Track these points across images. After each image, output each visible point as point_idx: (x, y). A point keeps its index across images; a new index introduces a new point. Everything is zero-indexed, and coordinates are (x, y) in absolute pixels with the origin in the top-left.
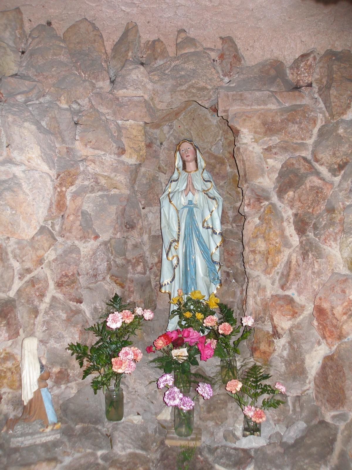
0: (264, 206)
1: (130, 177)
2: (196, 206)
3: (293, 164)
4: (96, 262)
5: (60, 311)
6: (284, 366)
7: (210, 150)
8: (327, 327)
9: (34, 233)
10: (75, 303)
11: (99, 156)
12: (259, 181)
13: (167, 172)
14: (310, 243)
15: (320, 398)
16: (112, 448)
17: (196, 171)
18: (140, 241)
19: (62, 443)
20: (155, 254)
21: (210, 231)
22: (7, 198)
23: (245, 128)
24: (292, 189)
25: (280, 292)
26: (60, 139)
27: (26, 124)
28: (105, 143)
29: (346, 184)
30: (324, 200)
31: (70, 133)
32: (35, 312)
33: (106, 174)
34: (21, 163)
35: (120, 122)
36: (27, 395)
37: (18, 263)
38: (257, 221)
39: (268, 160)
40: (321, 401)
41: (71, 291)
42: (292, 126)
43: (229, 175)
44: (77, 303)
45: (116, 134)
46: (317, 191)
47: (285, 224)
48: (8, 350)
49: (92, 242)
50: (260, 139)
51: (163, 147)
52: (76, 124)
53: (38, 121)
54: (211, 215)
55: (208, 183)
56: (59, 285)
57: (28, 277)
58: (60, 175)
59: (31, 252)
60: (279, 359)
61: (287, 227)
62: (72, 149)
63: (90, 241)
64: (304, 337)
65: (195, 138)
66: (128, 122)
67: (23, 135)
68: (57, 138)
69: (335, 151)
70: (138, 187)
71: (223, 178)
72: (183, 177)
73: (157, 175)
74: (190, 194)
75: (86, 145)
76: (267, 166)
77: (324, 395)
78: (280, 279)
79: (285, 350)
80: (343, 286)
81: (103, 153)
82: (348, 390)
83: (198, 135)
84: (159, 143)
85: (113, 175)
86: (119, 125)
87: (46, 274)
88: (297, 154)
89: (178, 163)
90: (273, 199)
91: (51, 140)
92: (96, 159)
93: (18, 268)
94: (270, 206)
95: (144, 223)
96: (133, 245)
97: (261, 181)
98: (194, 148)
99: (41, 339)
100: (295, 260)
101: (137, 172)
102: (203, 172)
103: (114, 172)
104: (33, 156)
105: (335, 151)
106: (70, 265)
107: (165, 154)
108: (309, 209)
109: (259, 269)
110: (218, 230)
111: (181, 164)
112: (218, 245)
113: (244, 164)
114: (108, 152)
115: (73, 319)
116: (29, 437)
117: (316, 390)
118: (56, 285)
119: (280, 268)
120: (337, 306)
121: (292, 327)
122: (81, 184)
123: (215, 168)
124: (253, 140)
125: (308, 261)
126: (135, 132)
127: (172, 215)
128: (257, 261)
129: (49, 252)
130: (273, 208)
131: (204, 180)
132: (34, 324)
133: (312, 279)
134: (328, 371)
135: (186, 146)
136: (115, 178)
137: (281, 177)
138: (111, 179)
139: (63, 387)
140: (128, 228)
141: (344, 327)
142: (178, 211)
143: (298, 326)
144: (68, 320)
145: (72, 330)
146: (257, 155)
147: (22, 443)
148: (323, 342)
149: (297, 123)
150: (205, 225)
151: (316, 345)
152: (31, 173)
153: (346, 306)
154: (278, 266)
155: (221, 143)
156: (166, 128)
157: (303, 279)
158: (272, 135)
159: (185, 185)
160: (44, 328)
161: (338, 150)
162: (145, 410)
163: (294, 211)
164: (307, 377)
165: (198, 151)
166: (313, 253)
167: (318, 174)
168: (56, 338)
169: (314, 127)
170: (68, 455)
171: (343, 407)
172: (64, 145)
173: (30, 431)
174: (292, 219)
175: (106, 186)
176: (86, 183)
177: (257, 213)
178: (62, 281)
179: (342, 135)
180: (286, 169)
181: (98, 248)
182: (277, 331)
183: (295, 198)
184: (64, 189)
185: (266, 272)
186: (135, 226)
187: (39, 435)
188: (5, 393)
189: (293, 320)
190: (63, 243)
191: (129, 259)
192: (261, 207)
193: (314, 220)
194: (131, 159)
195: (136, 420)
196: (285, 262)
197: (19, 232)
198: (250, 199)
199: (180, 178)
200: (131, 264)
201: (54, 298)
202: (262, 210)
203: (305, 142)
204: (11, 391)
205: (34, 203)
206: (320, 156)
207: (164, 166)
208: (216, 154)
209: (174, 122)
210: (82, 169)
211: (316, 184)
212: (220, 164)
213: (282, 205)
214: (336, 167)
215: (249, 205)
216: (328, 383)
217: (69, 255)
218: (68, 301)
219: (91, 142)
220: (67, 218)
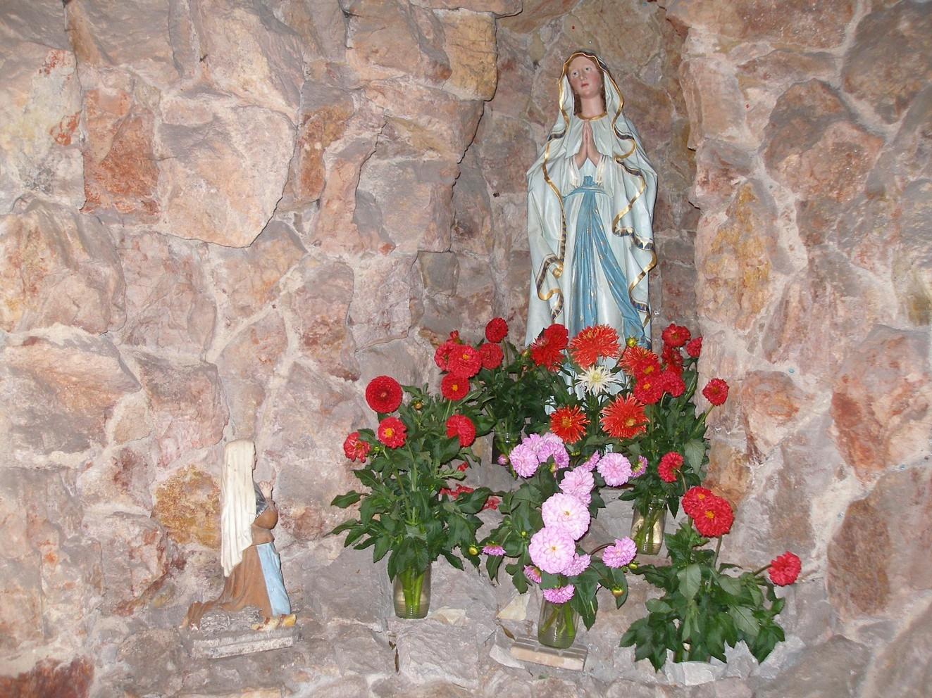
0: (737, 187)
1: (461, 127)
2: (600, 188)
3: (800, 98)
4: (386, 298)
5: (309, 394)
6: (768, 522)
7: (637, 75)
8: (857, 439)
9: (256, 233)
10: (342, 380)
11: (394, 81)
12: (728, 134)
13: (546, 120)
14: (828, 261)
15: (838, 590)
16: (397, 669)
17: (601, 116)
18: (487, 260)
19: (297, 654)
20: (519, 289)
21: (628, 239)
22: (200, 162)
23: (700, 23)
24: (797, 149)
25: (765, 366)
26: (313, 46)
27: (239, 13)
28: (406, 54)
29: (911, 137)
30: (863, 171)
31: (334, 34)
32: (260, 393)
33: (409, 118)
34: (231, 93)
35: (441, 13)
36: (231, 557)
37: (225, 295)
38: (723, 217)
39: (749, 90)
40: (839, 595)
41: (334, 354)
42: (801, 18)
43: (664, 123)
44: (346, 378)
45: (430, 37)
46: (848, 152)
47: (780, 223)
48: (200, 467)
49: (380, 256)
50: (733, 44)
51: (538, 70)
52: (348, 15)
53: (266, 8)
54: (630, 207)
55: (627, 141)
56: (310, 342)
57: (244, 323)
58: (309, 117)
59: (252, 274)
60: (759, 506)
61: (784, 231)
62: (338, 67)
63: (374, 255)
64: (810, 461)
65: (606, 50)
66: (457, 14)
67: (232, 35)
68: (305, 44)
69: (891, 68)
70: (487, 150)
71: (664, 134)
72: (575, 128)
73: (527, 128)
74: (589, 164)
75: (367, 59)
76: (747, 102)
77: (846, 583)
78: (765, 340)
79: (772, 487)
80: (894, 354)
81: (402, 73)
82: (896, 575)
83: (611, 45)
84: (530, 62)
85: (423, 121)
86: (437, 19)
87: (283, 319)
88: (810, 76)
89: (565, 98)
90: (756, 171)
91: (292, 47)
92: (388, 87)
93: (225, 306)
94: (750, 184)
95: (496, 226)
96: (472, 269)
97: (733, 135)
98: (598, 68)
99: (268, 449)
100: (797, 299)
101: (481, 119)
102: (616, 118)
103: (427, 113)
104: (254, 77)
105: (891, 68)
106: (331, 302)
107: (543, 85)
108: (831, 190)
109: (724, 317)
110: (646, 238)
111: (571, 102)
112: (646, 270)
113: (698, 99)
114: (412, 72)
115: (335, 410)
116: (230, 640)
117: (831, 573)
118: (302, 341)
119: (766, 315)
120: (881, 396)
121: (787, 440)
122: (356, 136)
123: (647, 112)
124: (718, 48)
125: (824, 301)
126: (472, 34)
127: (550, 207)
128: (720, 302)
129: (288, 275)
130: (756, 194)
131: (618, 134)
132: (256, 418)
133: (832, 339)
134: (858, 533)
135: (582, 63)
136: (429, 128)
137: (774, 126)
138: (422, 129)
139: (312, 545)
140: (462, 234)
141: (894, 441)
142: (562, 199)
143: (800, 439)
144: (325, 411)
145: (331, 431)
146: (726, 78)
147: (215, 650)
148: (851, 470)
149: (810, 11)
150: (619, 228)
151: (834, 478)
152: (250, 111)
153: (900, 396)
154: (763, 311)
155: (659, 60)
156: (545, 32)
157: (813, 339)
158: (758, 37)
159: (579, 144)
160: (276, 427)
161: (897, 67)
162: (474, 599)
163: (799, 196)
164: (814, 545)
165: (606, 75)
166: (835, 283)
167: (852, 117)
168: (299, 447)
169: (849, 20)
170: (307, 680)
171: (883, 609)
172: (322, 58)
173: (233, 628)
174: (795, 212)
175: (410, 143)
176: (367, 135)
177: (723, 201)
178: (316, 334)
179: (906, 34)
180: (785, 108)
181: (392, 270)
182: (756, 448)
183: (803, 169)
184: (318, 146)
185: (738, 323)
186: (477, 230)
187: (249, 637)
188: (193, 552)
189: (790, 424)
190: (319, 258)
191: (463, 296)
192: (732, 188)
193: (841, 215)
194: (464, 90)
195: (452, 617)
196: (777, 303)
197: (225, 231)
198: (707, 171)
199: (568, 131)
200: (468, 308)
201: (296, 367)
202: (734, 194)
203: (827, 51)
204: (205, 549)
205: (256, 174)
206: (857, 79)
207: (540, 109)
208: (648, 85)
209: (562, 19)
210: (357, 106)
211: (847, 139)
212: (657, 106)
213: (776, 184)
214: (892, 102)
215: (705, 183)
216: (855, 559)
217: (330, 282)
218: (326, 374)
219: (377, 52)
220: (326, 206)
